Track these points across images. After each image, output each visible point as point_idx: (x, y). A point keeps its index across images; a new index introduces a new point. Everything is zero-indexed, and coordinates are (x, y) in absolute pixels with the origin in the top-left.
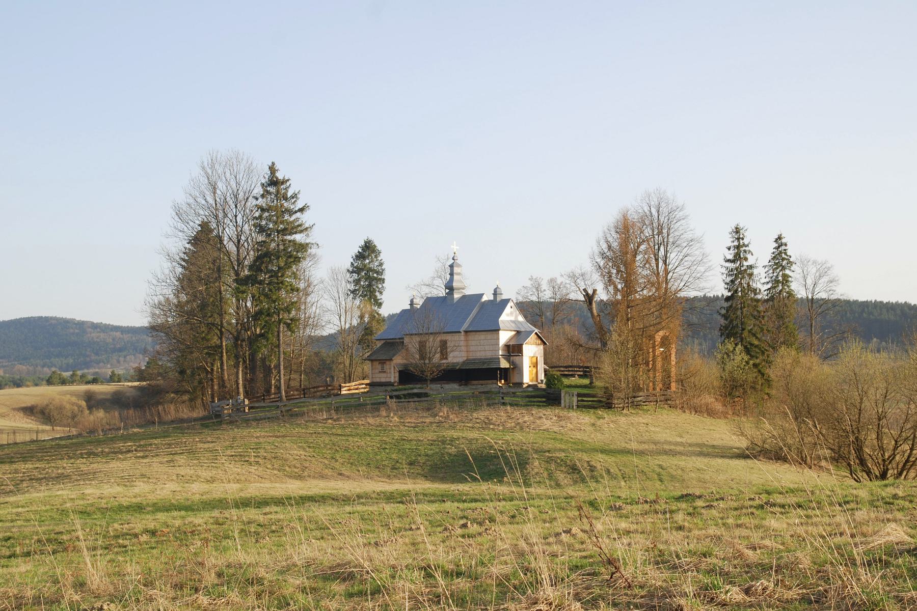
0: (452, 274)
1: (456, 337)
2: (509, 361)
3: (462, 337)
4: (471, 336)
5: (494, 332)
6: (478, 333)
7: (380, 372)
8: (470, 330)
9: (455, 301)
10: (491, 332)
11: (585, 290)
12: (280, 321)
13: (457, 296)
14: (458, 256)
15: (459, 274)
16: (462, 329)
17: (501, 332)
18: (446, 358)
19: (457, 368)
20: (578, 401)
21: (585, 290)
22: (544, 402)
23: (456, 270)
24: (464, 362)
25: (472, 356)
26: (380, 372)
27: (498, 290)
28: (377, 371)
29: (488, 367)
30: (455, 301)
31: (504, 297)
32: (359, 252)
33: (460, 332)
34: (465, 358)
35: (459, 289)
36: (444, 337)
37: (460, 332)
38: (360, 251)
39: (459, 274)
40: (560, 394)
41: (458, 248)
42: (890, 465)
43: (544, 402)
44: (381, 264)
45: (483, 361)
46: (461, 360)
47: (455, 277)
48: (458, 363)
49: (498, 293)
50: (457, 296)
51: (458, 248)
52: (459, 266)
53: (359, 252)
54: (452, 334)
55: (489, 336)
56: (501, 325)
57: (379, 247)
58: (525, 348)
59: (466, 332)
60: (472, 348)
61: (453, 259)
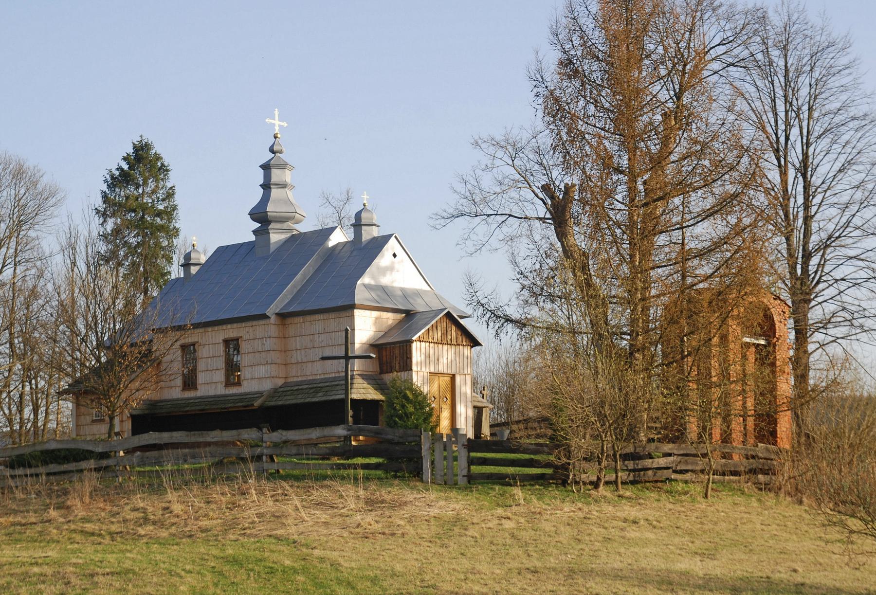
0: (266, 186)
1: (259, 329)
2: (380, 386)
3: (271, 328)
4: (296, 326)
5: (343, 314)
6: (308, 318)
7: (93, 421)
8: (291, 309)
9: (272, 248)
10: (337, 314)
11: (545, 188)
12: (786, 573)
13: (276, 237)
14: (283, 144)
15: (283, 185)
16: (271, 311)
17: (357, 313)
18: (239, 384)
19: (257, 404)
20: (471, 462)
21: (545, 188)
22: (377, 466)
23: (276, 175)
24: (275, 390)
25: (297, 375)
26: (93, 421)
27: (363, 215)
28: (88, 419)
29: (324, 398)
30: (272, 248)
31: (375, 232)
32: (120, 169)
33: (264, 317)
34: (280, 382)
35: (282, 220)
36: (231, 332)
37: (264, 317)
38: (125, 167)
39: (283, 185)
40: (419, 444)
41: (285, 124)
42: (699, 139)
43: (377, 466)
44: (170, 195)
45: (315, 386)
46: (267, 386)
47: (275, 192)
48: (260, 394)
49: (363, 222)
50: (276, 237)
51: (285, 124)
52: (283, 166)
53: (120, 169)
54: (250, 323)
55: (333, 322)
56: (361, 295)
57: (167, 159)
58: (418, 352)
59: (283, 316)
60: (297, 357)
61: (272, 150)
